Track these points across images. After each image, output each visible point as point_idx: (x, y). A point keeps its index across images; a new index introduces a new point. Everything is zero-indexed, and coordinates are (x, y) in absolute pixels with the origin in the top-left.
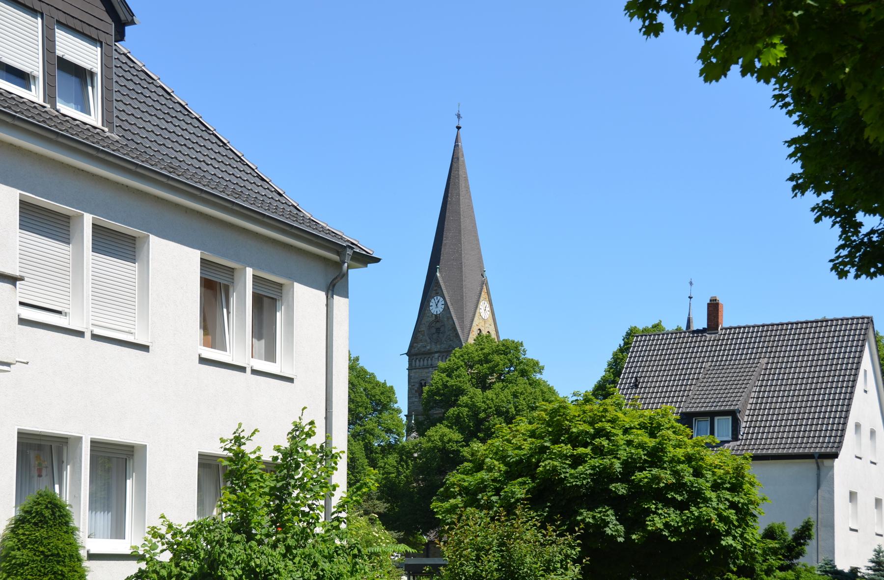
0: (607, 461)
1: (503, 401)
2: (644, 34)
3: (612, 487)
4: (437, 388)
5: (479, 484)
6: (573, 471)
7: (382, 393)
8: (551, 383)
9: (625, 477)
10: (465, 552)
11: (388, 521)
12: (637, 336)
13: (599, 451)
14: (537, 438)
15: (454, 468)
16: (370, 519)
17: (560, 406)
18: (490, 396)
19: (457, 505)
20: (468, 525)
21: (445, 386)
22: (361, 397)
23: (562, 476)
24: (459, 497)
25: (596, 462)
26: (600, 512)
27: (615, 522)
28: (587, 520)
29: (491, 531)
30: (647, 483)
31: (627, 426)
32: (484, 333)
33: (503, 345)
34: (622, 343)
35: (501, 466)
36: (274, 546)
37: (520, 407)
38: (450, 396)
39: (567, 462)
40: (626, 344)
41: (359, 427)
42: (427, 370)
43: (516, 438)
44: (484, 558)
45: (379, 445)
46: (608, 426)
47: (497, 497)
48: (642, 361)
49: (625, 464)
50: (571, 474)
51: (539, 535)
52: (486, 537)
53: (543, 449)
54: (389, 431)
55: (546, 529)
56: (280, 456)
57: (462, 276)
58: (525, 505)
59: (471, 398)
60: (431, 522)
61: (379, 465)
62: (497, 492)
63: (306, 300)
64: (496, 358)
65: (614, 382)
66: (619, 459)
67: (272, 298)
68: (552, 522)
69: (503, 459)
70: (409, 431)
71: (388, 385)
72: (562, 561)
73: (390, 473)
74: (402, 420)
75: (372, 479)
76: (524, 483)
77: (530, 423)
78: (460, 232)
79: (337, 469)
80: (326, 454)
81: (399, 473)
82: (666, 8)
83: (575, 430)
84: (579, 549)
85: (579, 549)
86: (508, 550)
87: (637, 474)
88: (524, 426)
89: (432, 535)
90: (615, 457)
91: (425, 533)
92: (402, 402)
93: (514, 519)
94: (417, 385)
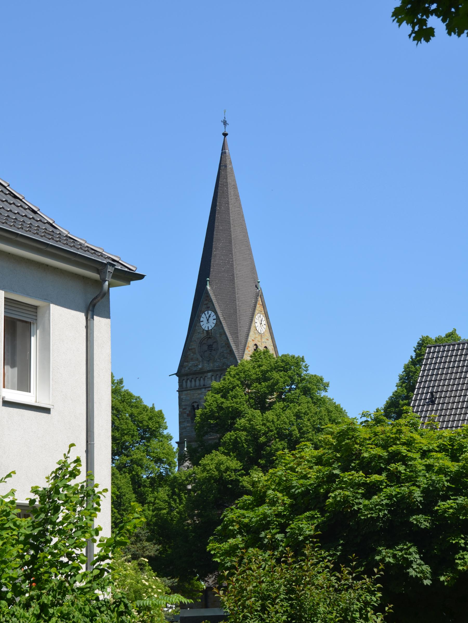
0: (405, 489)
1: (285, 423)
2: (414, 39)
3: (413, 519)
4: (212, 411)
5: (261, 520)
6: (367, 502)
7: (150, 419)
8: (337, 401)
9: (427, 507)
10: (248, 602)
11: (159, 566)
12: (430, 348)
13: (395, 478)
14: (324, 465)
15: (232, 502)
16: (139, 564)
17: (348, 429)
18: (270, 418)
19: (237, 545)
20: (250, 569)
21: (220, 408)
22: (126, 423)
23: (356, 508)
24: (239, 536)
25: (393, 490)
26: (401, 550)
27: (419, 561)
28: (387, 559)
29: (277, 575)
30: (453, 514)
31: (425, 448)
32: (261, 348)
33: (283, 361)
34: (414, 355)
35: (286, 498)
36: (27, 606)
37: (304, 429)
38: (225, 419)
39: (360, 491)
40: (417, 355)
41: (125, 458)
42: (199, 392)
43: (301, 466)
44: (271, 609)
45: (148, 478)
46: (403, 450)
47: (282, 535)
48: (437, 375)
49: (425, 492)
50: (365, 506)
51: (333, 578)
52: (271, 583)
53: (332, 478)
54: (158, 460)
55: (341, 572)
56: (38, 500)
57: (234, 288)
58: (314, 543)
59: (250, 420)
60: (208, 566)
61: (149, 499)
62: (282, 528)
63: (64, 323)
64: (276, 375)
65: (408, 398)
66: (419, 487)
67: (26, 322)
68: (347, 563)
69: (286, 489)
70: (181, 460)
71: (157, 409)
72: (361, 609)
73: (161, 509)
74: (170, 449)
75: (138, 517)
76: (312, 518)
77: (316, 448)
78: (230, 242)
79: (99, 510)
80: (89, 494)
81: (171, 509)
82: (436, 12)
83: (366, 455)
84: (379, 595)
85: (379, 595)
86: (297, 598)
87: (440, 503)
88: (309, 452)
89: (211, 580)
90: (414, 485)
91: (202, 578)
92: (172, 428)
93: (303, 561)
94: (189, 409)
